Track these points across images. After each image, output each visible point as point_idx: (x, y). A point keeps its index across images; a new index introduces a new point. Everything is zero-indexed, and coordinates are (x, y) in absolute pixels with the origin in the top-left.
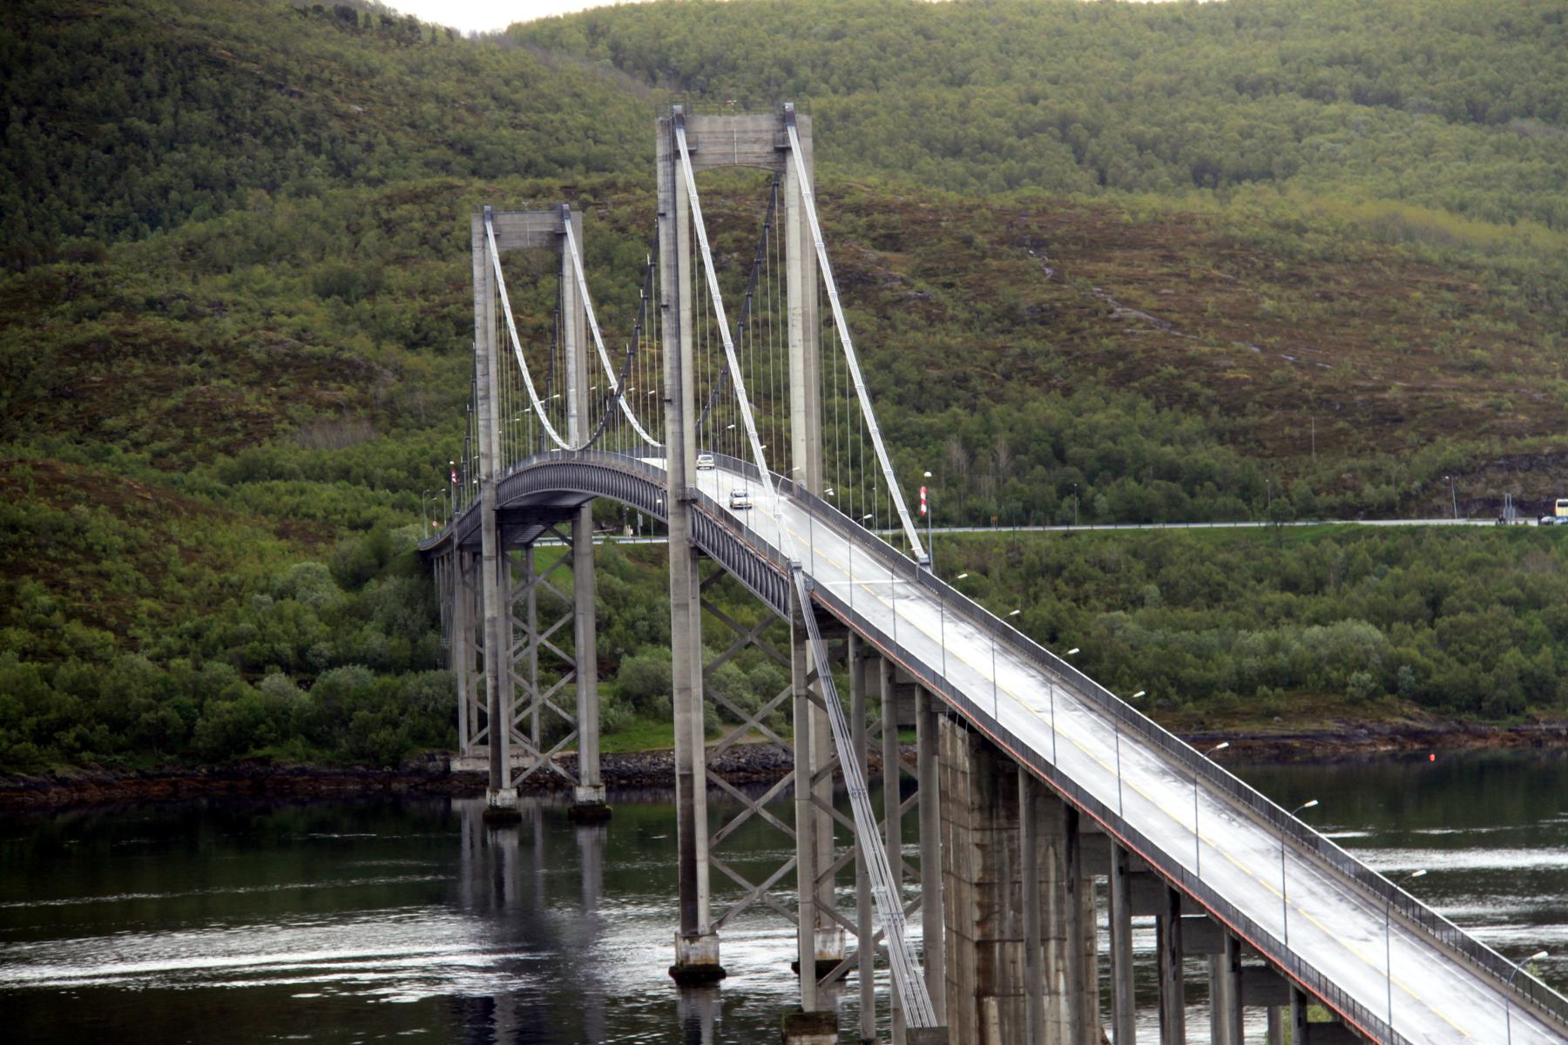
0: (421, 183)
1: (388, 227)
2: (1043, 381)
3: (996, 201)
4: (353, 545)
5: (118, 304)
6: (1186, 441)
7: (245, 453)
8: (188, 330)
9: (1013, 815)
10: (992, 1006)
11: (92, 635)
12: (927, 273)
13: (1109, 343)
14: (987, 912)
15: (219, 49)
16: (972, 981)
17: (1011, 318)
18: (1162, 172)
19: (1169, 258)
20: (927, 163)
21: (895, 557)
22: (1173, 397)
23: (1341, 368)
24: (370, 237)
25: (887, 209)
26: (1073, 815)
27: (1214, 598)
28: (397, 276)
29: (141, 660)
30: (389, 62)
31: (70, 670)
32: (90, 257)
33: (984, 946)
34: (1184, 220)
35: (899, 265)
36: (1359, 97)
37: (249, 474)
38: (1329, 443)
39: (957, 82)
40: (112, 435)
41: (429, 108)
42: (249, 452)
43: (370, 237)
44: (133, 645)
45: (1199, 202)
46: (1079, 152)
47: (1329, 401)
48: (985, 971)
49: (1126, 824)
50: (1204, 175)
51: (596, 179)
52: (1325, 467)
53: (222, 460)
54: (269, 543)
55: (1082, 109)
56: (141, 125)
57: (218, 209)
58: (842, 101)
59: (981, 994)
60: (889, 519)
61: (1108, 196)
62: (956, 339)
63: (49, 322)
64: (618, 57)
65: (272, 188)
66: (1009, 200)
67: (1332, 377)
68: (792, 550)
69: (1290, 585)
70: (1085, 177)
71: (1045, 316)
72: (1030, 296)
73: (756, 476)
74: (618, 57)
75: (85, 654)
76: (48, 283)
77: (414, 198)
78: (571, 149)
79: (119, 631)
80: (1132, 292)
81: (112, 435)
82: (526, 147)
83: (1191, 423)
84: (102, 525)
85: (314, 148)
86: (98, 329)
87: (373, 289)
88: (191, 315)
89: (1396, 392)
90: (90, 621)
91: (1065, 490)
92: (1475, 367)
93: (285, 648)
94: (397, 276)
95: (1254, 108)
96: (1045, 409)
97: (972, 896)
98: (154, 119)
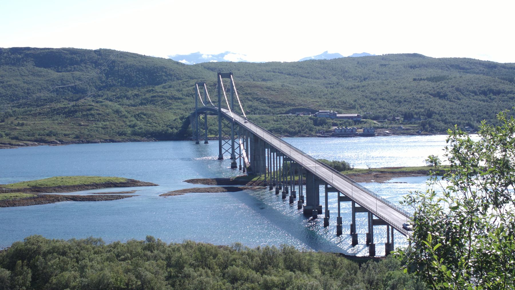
1: (183, 84)
5: (157, 92)
6: (264, 107)
8: (164, 94)
10: (255, 162)
11: (156, 125)
13: (256, 97)
15: (165, 67)
17: (246, 94)
19: (262, 88)
23: (279, 100)
24: (181, 85)
28: (184, 89)
31: (154, 128)
34: (263, 85)
36: (279, 72)
37: (170, 109)
38: (278, 107)
39: (239, 70)
40: (156, 105)
41: (186, 73)
46: (251, 77)
47: (278, 103)
49: (360, 170)
50: (264, 80)
52: (278, 109)
53: (167, 107)
54: (173, 116)
59: (254, 160)
61: (254, 82)
63: (508, 152)
68: (232, 117)
69: (275, 121)
70: (252, 80)
71: (250, 94)
72: (249, 91)
74: (205, 68)
75: (155, 127)
79: (159, 124)
80: (258, 91)
81: (156, 105)
83: (264, 105)
85: (175, 77)
86: (155, 94)
88: (164, 93)
89: (285, 102)
91: (252, 111)
92: (292, 100)
95: (269, 73)
96: (250, 103)
98: (159, 73)
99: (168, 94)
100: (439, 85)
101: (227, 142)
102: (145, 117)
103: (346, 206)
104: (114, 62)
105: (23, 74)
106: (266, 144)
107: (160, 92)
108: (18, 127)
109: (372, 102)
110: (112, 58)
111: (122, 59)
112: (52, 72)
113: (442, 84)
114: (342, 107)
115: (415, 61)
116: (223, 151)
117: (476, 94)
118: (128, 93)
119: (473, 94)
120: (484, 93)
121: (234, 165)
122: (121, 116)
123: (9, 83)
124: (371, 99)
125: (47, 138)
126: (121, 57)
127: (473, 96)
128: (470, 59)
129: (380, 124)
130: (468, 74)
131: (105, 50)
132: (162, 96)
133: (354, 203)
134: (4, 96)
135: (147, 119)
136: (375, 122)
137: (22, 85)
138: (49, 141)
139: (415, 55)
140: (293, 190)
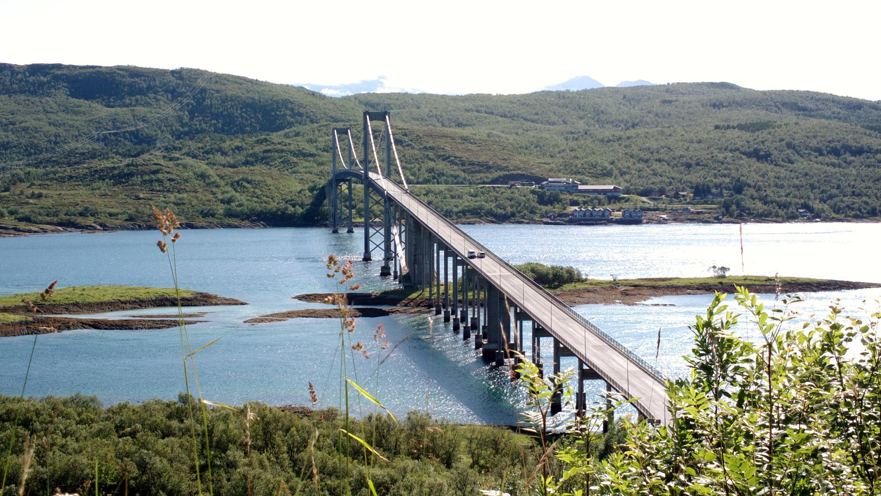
0: (325, 123)
1: (319, 130)
2: (432, 160)
3: (424, 128)
4: (311, 184)
5: (273, 143)
7: (294, 169)
8: (284, 148)
9: (420, 233)
10: (416, 266)
12: (411, 141)
13: (442, 153)
14: (416, 250)
16: (413, 262)
18: (453, 124)
20: (413, 122)
21: (399, 183)
22: (453, 163)
24: (316, 132)
25: (405, 129)
26: (430, 233)
27: (459, 197)
29: (275, 204)
30: (321, 103)
32: (268, 135)
33: (415, 255)
35: (406, 139)
36: (486, 112)
37: (294, 172)
38: (480, 172)
40: (271, 166)
41: (327, 110)
42: (294, 169)
43: (316, 132)
44: (274, 202)
45: (459, 130)
47: (479, 164)
48: (415, 260)
49: (599, 283)
50: (460, 125)
51: (355, 123)
52: (479, 176)
53: (290, 170)
55: (439, 113)
56: (278, 113)
57: (291, 127)
58: (398, 111)
59: (414, 264)
60: (401, 183)
62: (416, 152)
64: (360, 102)
65: (300, 124)
66: (425, 128)
67: (480, 160)
70: (440, 125)
71: (432, 148)
72: (431, 144)
73: (377, 173)
75: (266, 202)
76: (533, 271)
77: (323, 126)
78: (351, 118)
79: (272, 198)
81: (271, 166)
82: (343, 117)
83: (456, 167)
84: (269, 181)
86: (269, 147)
87: (316, 141)
88: (285, 145)
89: (491, 163)
90: (267, 197)
91: (434, 178)
93: (300, 203)
94: (321, 139)
95: (469, 114)
96: (431, 164)
97: (413, 247)
98: (281, 111)
99: (292, 147)
100: (758, 136)
101: (378, 231)
102: (249, 186)
103: (569, 366)
104: (203, 90)
105: (49, 110)
106: (432, 237)
107: (279, 143)
108: (31, 201)
109: (640, 165)
110: (201, 83)
111: (218, 87)
112: (99, 107)
113: (763, 135)
114: (589, 173)
115: (722, 95)
116: (372, 246)
117: (821, 154)
118: (223, 145)
119: (817, 154)
120: (835, 152)
121: (385, 271)
122: (208, 184)
123: (23, 125)
124: (641, 160)
125: (80, 220)
126: (216, 82)
127: (816, 157)
128: (817, 94)
129: (651, 204)
130: (812, 119)
131: (190, 71)
132: (282, 151)
133: (534, 322)
134: (15, 147)
135: (252, 190)
136: (644, 199)
137: (47, 128)
138: (83, 224)
139: (723, 85)
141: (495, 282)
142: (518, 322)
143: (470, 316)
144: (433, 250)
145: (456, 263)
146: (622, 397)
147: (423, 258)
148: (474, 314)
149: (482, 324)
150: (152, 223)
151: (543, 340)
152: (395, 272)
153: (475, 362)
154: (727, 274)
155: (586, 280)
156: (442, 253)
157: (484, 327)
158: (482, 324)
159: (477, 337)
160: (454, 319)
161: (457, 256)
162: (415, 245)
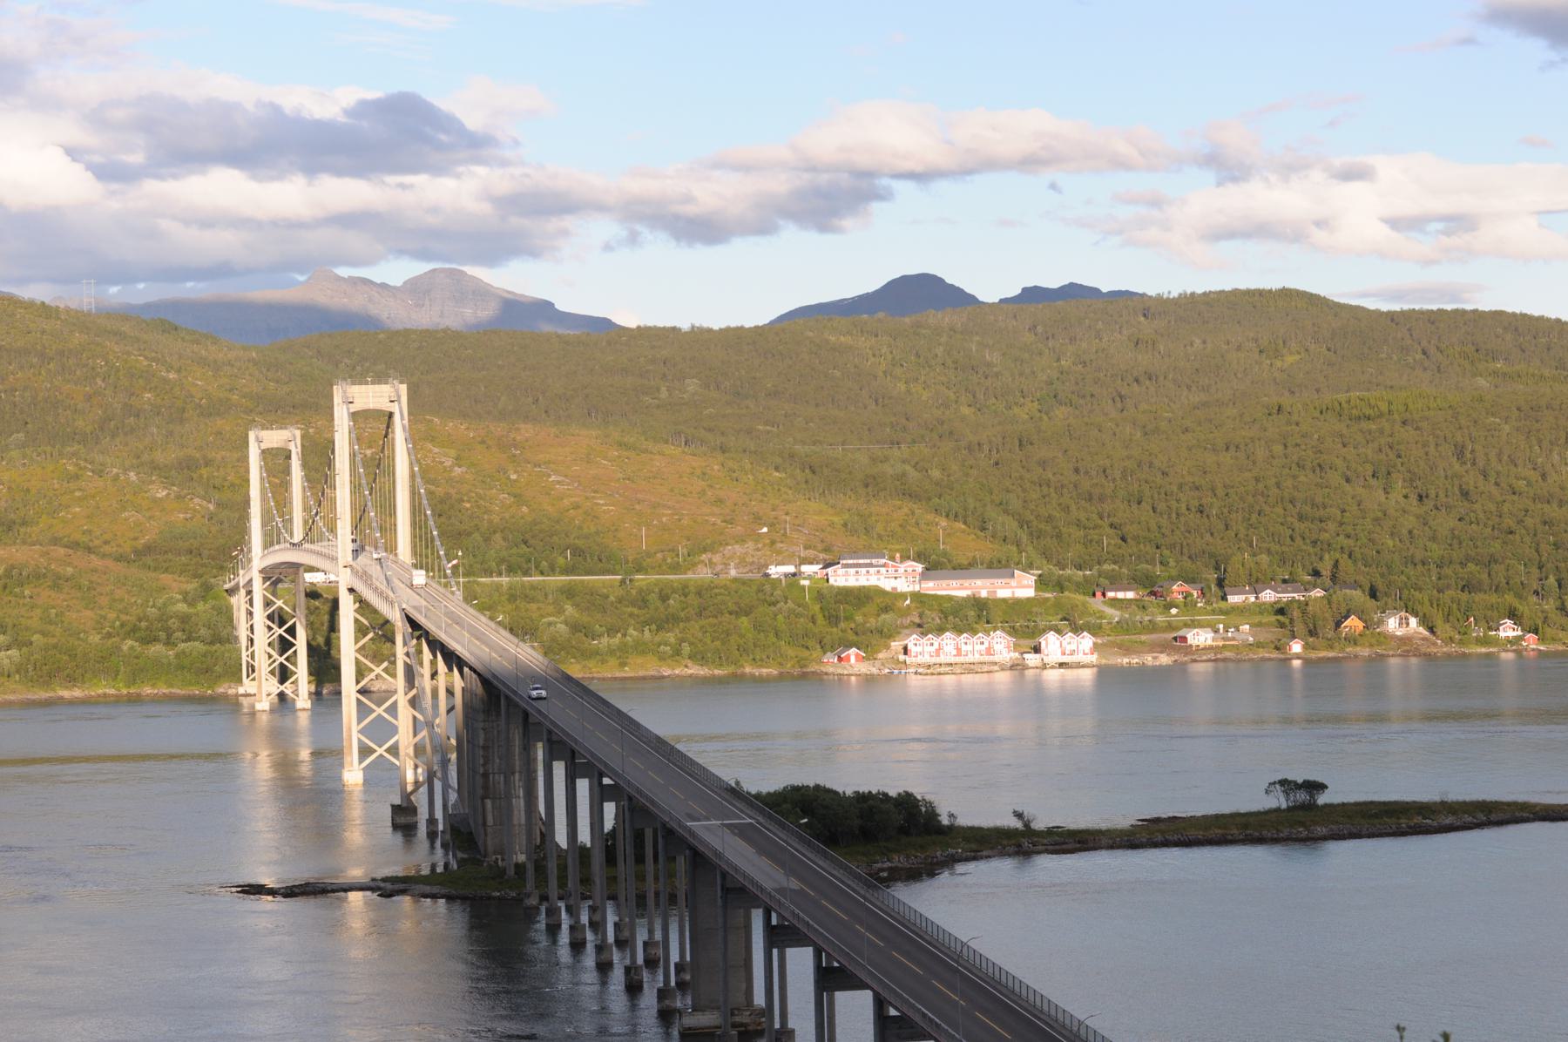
9: (498, 714)
10: (489, 803)
48: (486, 787)
140: (777, 1026)
141: (707, 845)
142: (775, 951)
143: (641, 936)
144: (1049, 1033)
145: (600, 795)
146: (684, 891)
147: (507, 781)
148: (651, 932)
149: (674, 957)
150: (1113, 602)
151: (842, 998)
152: (432, 821)
153: (433, 768)
154: (1323, 799)
155: (951, 828)
156: (559, 769)
157: (680, 968)
158: (674, 957)
159: (663, 994)
160: (628, 970)
161: (601, 775)
162: (485, 748)
